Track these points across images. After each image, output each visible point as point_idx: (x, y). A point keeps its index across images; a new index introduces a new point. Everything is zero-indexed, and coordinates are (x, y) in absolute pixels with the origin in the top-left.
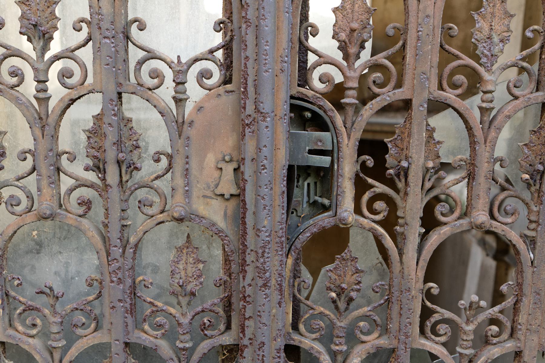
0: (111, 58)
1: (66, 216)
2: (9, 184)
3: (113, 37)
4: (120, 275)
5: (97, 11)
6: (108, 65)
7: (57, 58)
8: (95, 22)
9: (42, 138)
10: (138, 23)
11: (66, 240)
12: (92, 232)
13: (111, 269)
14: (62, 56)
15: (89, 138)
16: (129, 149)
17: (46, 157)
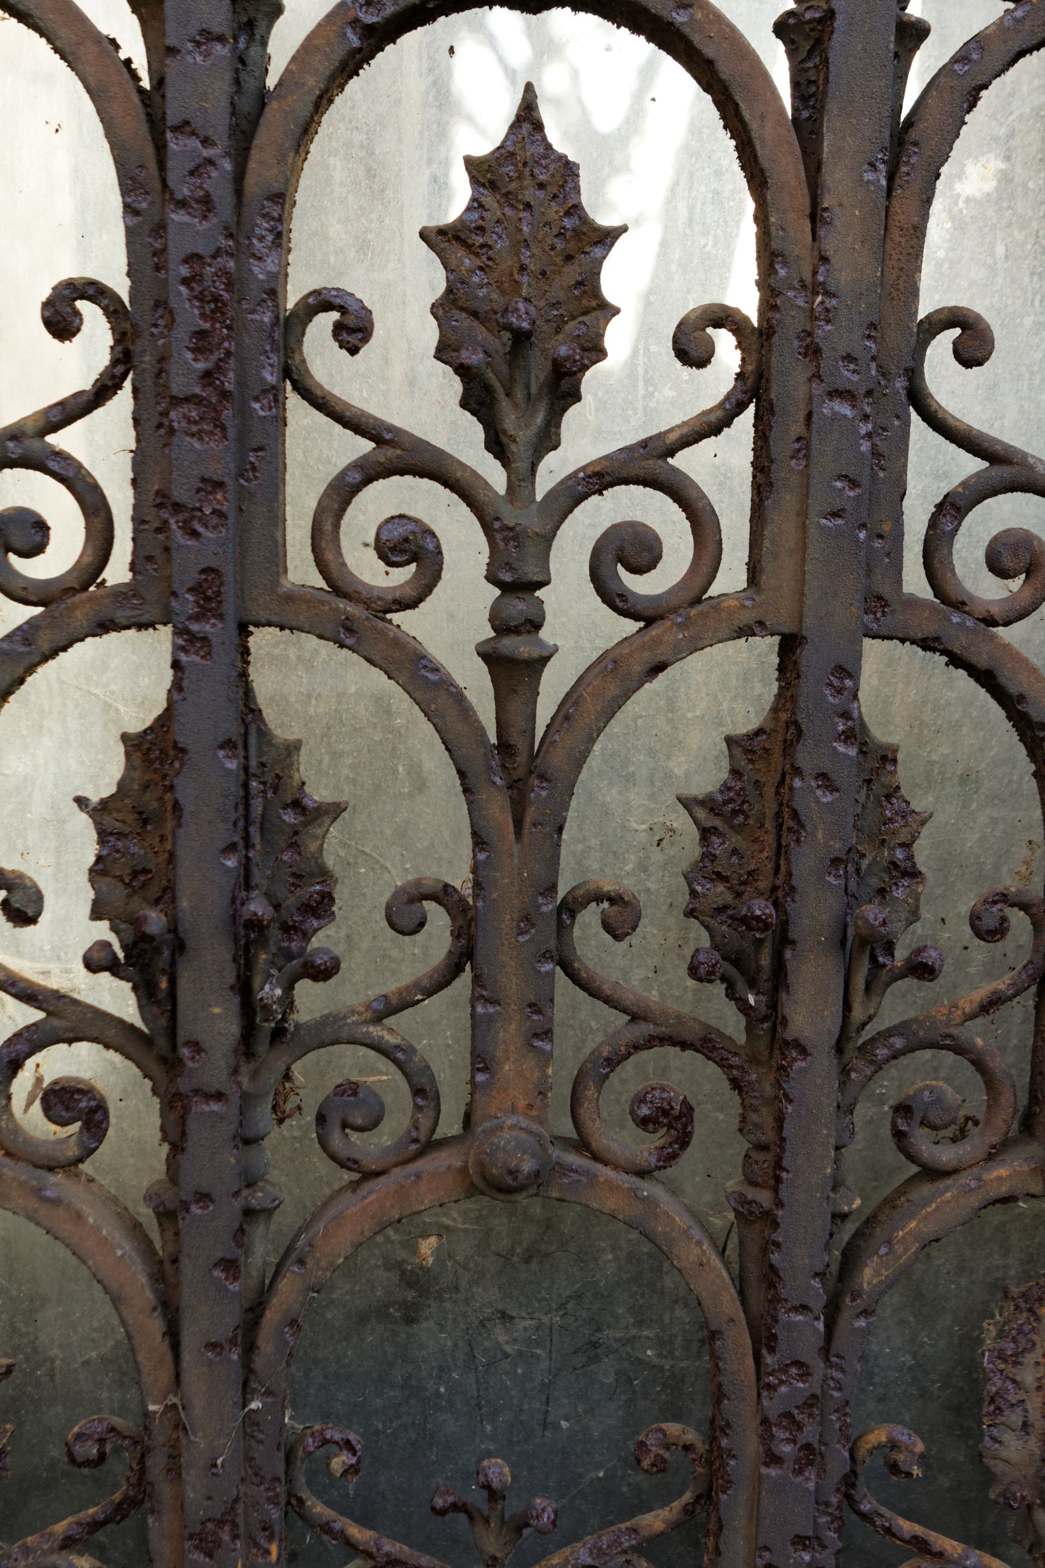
0: (854, 484)
1: (592, 1177)
2: (344, 1035)
3: (869, 393)
4: (810, 1433)
5: (807, 276)
6: (835, 515)
7: (598, 479)
8: (792, 322)
9: (512, 837)
10: (958, 331)
11: (534, 1266)
12: (699, 1243)
13: (772, 1406)
14: (624, 473)
15: (706, 833)
16: (874, 882)
17: (526, 918)
